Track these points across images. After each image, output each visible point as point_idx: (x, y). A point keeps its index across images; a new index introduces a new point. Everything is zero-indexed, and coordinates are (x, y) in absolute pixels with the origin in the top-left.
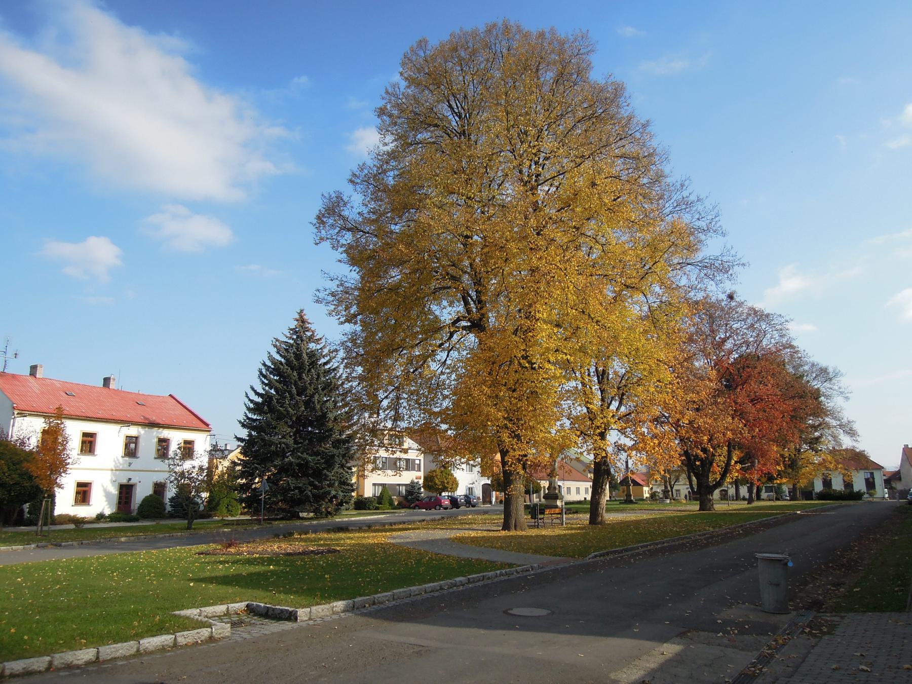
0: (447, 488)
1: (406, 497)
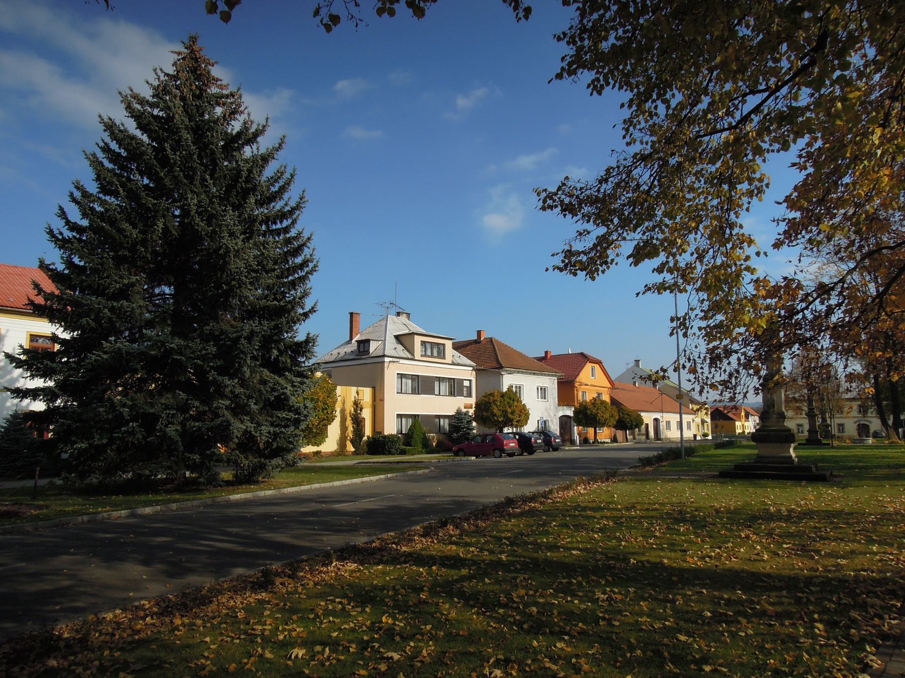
0: (512, 421)
1: (449, 435)
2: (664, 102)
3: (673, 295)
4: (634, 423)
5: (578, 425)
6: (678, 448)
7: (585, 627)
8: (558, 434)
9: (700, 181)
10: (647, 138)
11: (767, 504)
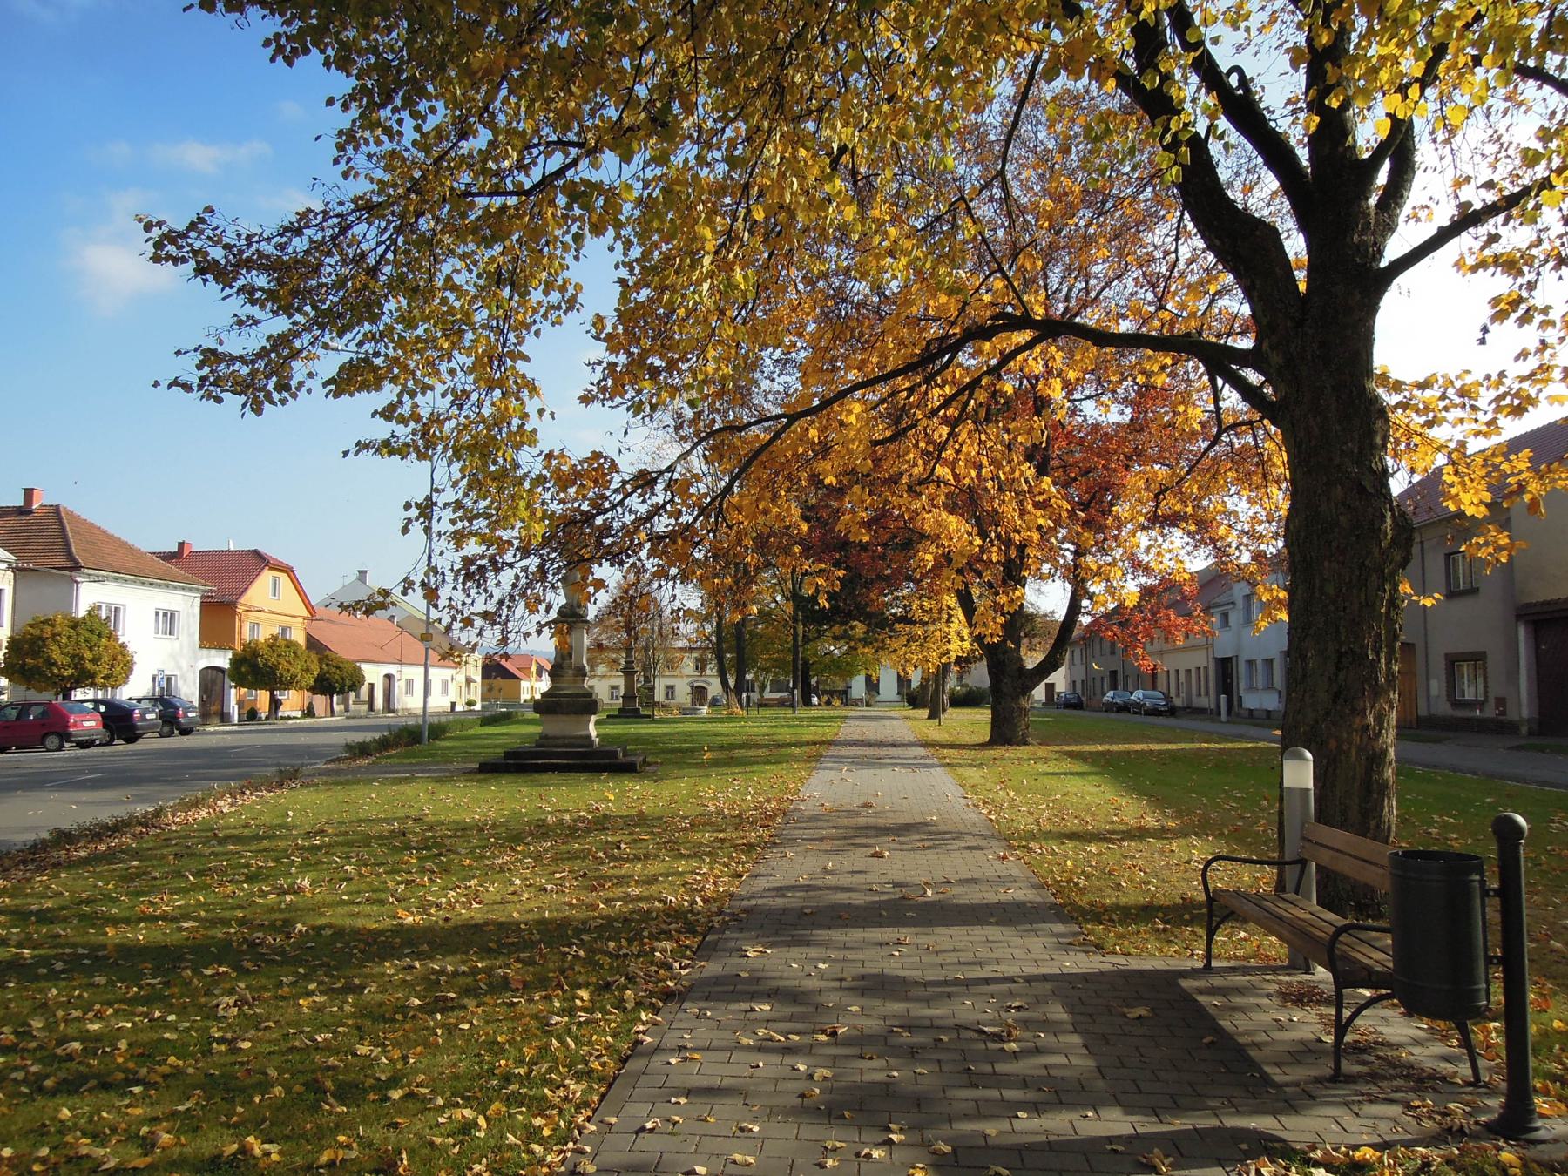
0: (92, 676)
2: (415, 115)
3: (426, 464)
4: (348, 683)
5: (239, 685)
6: (418, 726)
7: (180, 1063)
8: (196, 704)
9: (470, 272)
10: (379, 174)
11: (544, 812)
